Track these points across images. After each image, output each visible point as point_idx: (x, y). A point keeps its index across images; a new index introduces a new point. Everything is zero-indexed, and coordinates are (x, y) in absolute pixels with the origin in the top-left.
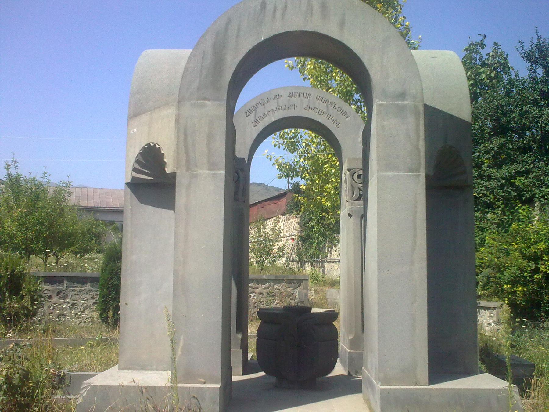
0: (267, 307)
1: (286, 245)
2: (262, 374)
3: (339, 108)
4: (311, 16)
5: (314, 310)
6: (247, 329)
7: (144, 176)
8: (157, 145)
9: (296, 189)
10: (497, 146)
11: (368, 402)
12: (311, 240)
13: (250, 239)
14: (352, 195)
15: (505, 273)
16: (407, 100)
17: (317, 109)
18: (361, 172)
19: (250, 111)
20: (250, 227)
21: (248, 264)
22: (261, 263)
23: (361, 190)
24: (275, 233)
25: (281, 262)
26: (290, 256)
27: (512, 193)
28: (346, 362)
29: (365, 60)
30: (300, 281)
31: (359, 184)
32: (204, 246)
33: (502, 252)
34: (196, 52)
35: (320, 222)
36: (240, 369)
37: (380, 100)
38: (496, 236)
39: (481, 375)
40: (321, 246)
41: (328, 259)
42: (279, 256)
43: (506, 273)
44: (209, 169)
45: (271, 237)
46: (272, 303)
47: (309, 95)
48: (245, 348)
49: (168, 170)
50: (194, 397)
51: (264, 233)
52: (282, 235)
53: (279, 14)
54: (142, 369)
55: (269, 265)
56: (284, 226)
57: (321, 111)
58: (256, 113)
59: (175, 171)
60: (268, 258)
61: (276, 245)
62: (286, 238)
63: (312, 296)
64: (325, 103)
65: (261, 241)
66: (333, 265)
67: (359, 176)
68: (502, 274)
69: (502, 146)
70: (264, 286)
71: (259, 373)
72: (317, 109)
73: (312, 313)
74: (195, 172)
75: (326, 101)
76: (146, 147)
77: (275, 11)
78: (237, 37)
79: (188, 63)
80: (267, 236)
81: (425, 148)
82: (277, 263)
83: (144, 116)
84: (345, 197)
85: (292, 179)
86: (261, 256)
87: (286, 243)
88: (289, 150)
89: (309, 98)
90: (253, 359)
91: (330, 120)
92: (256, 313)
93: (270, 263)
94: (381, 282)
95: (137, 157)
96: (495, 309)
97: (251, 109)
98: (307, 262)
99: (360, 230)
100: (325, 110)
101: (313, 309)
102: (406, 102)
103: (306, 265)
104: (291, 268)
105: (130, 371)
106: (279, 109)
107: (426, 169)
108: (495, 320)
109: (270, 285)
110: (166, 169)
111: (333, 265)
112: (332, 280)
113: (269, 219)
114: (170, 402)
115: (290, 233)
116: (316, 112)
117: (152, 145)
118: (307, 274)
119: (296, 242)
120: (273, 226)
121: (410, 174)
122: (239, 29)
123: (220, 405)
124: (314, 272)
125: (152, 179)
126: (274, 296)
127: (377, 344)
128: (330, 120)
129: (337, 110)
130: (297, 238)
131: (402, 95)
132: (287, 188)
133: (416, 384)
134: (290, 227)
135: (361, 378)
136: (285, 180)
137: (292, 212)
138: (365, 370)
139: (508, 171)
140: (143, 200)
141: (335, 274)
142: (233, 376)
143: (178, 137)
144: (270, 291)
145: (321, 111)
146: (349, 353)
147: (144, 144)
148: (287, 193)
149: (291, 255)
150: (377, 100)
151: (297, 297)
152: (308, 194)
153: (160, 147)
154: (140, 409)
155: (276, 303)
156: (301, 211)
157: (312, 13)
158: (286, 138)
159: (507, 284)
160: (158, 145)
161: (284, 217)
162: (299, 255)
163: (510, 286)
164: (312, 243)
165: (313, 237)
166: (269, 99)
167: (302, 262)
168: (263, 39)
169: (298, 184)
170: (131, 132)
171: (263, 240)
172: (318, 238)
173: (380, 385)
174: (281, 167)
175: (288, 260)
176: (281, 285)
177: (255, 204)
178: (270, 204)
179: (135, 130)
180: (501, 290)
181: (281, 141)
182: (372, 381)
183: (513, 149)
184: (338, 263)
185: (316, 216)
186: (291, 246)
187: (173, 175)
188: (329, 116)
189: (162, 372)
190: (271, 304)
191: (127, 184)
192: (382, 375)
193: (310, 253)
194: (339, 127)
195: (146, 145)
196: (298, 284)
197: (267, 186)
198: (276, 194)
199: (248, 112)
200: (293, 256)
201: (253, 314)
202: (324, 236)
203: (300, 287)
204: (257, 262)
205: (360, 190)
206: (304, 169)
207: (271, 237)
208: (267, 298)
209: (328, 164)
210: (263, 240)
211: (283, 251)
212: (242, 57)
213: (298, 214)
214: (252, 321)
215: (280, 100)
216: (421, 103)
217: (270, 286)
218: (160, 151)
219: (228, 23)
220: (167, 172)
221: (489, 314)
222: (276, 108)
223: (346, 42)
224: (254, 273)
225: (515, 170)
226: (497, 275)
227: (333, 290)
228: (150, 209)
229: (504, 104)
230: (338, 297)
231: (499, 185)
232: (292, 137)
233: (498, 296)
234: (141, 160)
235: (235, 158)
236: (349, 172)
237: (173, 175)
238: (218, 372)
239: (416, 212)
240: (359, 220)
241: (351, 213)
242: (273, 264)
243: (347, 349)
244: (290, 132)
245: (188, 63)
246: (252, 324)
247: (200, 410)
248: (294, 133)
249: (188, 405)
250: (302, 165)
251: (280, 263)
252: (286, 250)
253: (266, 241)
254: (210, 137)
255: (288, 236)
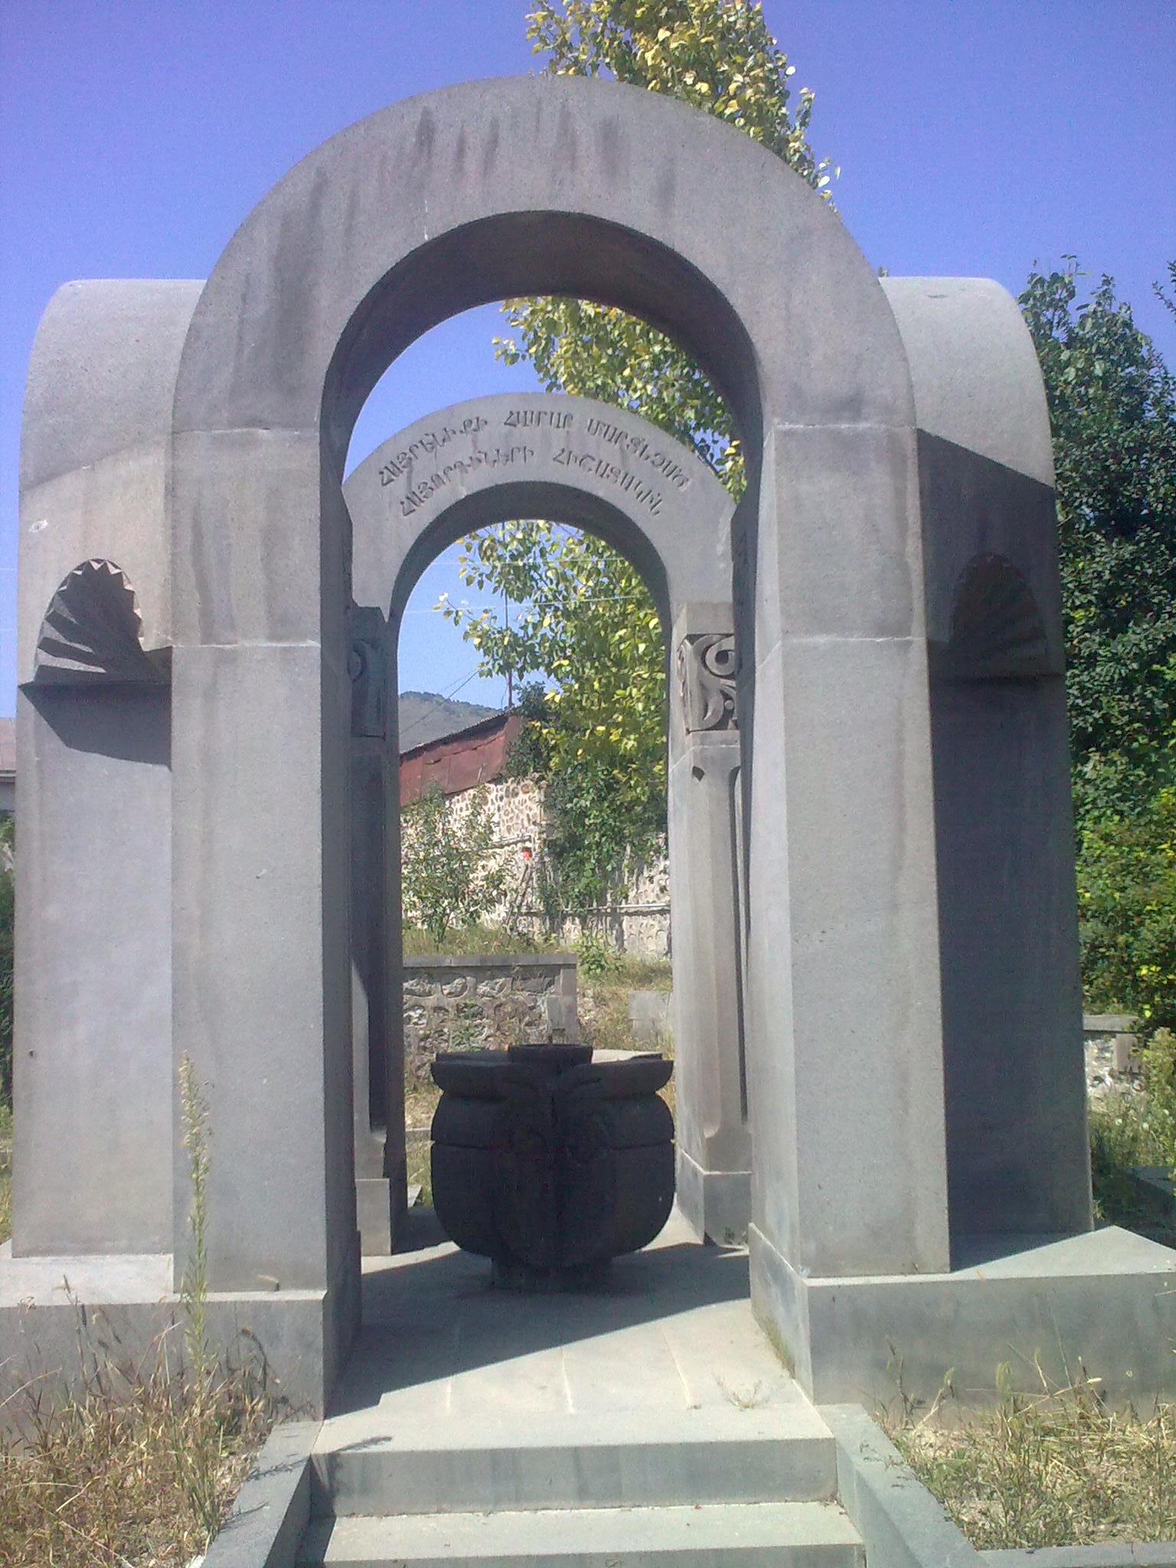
0: (458, 1048)
1: (509, 867)
2: (450, 1247)
3: (656, 455)
4: (573, 168)
5: (601, 1056)
6: (403, 1113)
7: (77, 663)
8: (110, 566)
9: (535, 707)
10: (1112, 567)
11: (770, 1328)
12: (578, 853)
13: (403, 853)
14: (702, 712)
15: (1144, 932)
16: (866, 419)
17: (593, 459)
18: (729, 644)
19: (393, 469)
20: (402, 819)
21: (398, 925)
22: (437, 921)
23: (731, 699)
24: (476, 834)
25: (494, 916)
26: (519, 898)
27: (1157, 702)
28: (696, 1207)
29: (738, 301)
30: (551, 971)
31: (723, 681)
32: (264, 871)
33: (1130, 873)
34: (222, 278)
35: (605, 799)
36: (386, 1235)
37: (785, 418)
38: (1114, 828)
39: (1098, 1232)
40: (609, 868)
41: (631, 905)
42: (488, 901)
43: (1145, 931)
44: (273, 637)
45: (463, 845)
46: (472, 1035)
47: (568, 417)
48: (396, 1173)
49: (148, 643)
50: (245, 1332)
51: (445, 834)
52: (495, 838)
53: (472, 162)
54: (87, 1251)
55: (460, 926)
56: (502, 812)
57: (603, 464)
58: (410, 472)
59: (169, 645)
60: (457, 907)
61: (480, 868)
62: (506, 848)
63: (588, 1012)
64: (616, 442)
65: (436, 858)
66: (645, 922)
67: (722, 657)
68: (1136, 935)
69: (1123, 569)
70: (447, 989)
71: (440, 1246)
72: (593, 459)
73: (596, 1066)
74: (227, 647)
75: (617, 437)
76: (79, 573)
77: (461, 152)
78: (349, 230)
79: (200, 313)
80: (452, 843)
81: (925, 562)
82: (482, 918)
83: (68, 479)
84: (681, 719)
85: (521, 677)
86: (437, 902)
87: (507, 861)
88: (509, 593)
89: (569, 426)
90: (422, 1204)
91: (632, 492)
92: (427, 1067)
93: (464, 921)
94: (800, 969)
95: (51, 605)
96: (1114, 1037)
97: (396, 462)
98: (571, 915)
99: (728, 817)
100: (616, 463)
101: (596, 1053)
102: (862, 426)
103: (568, 925)
104: (525, 935)
105: (49, 1259)
106: (480, 461)
107: (927, 626)
108: (1116, 1068)
109: (465, 983)
110: (141, 639)
111: (645, 922)
112: (644, 965)
113: (458, 793)
114: (172, 1352)
115: (518, 832)
116: (590, 470)
117: (96, 566)
118: (570, 951)
119: (537, 859)
120: (468, 813)
121: (881, 640)
122: (352, 211)
123: (325, 1354)
124: (590, 944)
125: (101, 670)
126: (479, 1014)
127: (794, 1158)
128: (632, 492)
129: (653, 462)
130: (540, 847)
131: (852, 405)
132: (507, 705)
133: (915, 1271)
134: (518, 817)
135: (744, 1251)
136: (500, 681)
137: (525, 774)
138: (758, 1231)
139: (1146, 637)
140: (75, 737)
141: (652, 947)
142: (363, 1259)
143: (175, 539)
144: (468, 1002)
145: (603, 464)
146: (707, 1178)
147: (70, 565)
148: (506, 719)
149: (524, 895)
150: (776, 420)
151: (545, 1016)
152: (567, 718)
153: (120, 574)
154: (81, 1378)
155: (483, 1036)
156: (550, 770)
157: (573, 158)
158: (499, 558)
159: (1148, 963)
160: (116, 567)
161: (499, 787)
162: (548, 896)
163: (1159, 969)
164: (582, 862)
165: (586, 843)
166: (450, 433)
167: (554, 917)
168: (426, 237)
169: (539, 690)
170: (32, 529)
171: (442, 855)
172: (598, 844)
173: (809, 1277)
174: (487, 643)
175: (516, 910)
176: (496, 983)
177: (416, 753)
178: (460, 749)
179: (45, 524)
180: (1133, 981)
181: (486, 567)
182: (783, 1263)
183: (1154, 579)
184: (658, 915)
185: (592, 781)
186: (522, 870)
187: (165, 656)
188: (628, 481)
189: (150, 1257)
190: (471, 1038)
191: (24, 688)
192: (812, 1247)
193: (577, 890)
194: (658, 512)
195: (78, 569)
196: (548, 979)
197: (448, 701)
198: (475, 721)
199: (385, 471)
200: (530, 899)
201: (419, 1068)
202: (618, 838)
203: (552, 989)
204: (427, 918)
205: (727, 697)
206: (556, 648)
207: (463, 845)
208: (459, 1023)
209: (626, 627)
210: (442, 855)
211: (498, 885)
212: (365, 292)
213: (542, 778)
214: (415, 1089)
215: (481, 434)
216: (907, 428)
217: (464, 987)
218: (122, 584)
219: (320, 188)
220: (146, 648)
221: (1096, 1051)
222: (471, 458)
223: (679, 247)
224: (418, 949)
225: (1165, 634)
226: (1121, 939)
227: (648, 993)
228: (99, 764)
229: (1132, 444)
230: (662, 1015)
231: (1124, 675)
232: (516, 553)
233: (1122, 1000)
234: (66, 613)
235: (350, 605)
236: (692, 644)
237: (165, 656)
238: (316, 1251)
239: (900, 756)
240: (726, 783)
241: (700, 767)
242: (472, 923)
243: (700, 1169)
244: (507, 531)
245: (198, 312)
246: (415, 1098)
247: (264, 1369)
248: (521, 542)
249: (227, 1357)
250: (550, 635)
251: (492, 920)
252: (509, 883)
253: (449, 857)
254: (272, 537)
255: (513, 843)
